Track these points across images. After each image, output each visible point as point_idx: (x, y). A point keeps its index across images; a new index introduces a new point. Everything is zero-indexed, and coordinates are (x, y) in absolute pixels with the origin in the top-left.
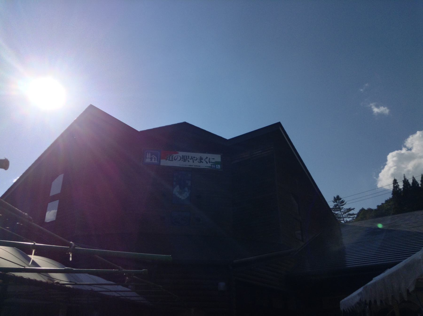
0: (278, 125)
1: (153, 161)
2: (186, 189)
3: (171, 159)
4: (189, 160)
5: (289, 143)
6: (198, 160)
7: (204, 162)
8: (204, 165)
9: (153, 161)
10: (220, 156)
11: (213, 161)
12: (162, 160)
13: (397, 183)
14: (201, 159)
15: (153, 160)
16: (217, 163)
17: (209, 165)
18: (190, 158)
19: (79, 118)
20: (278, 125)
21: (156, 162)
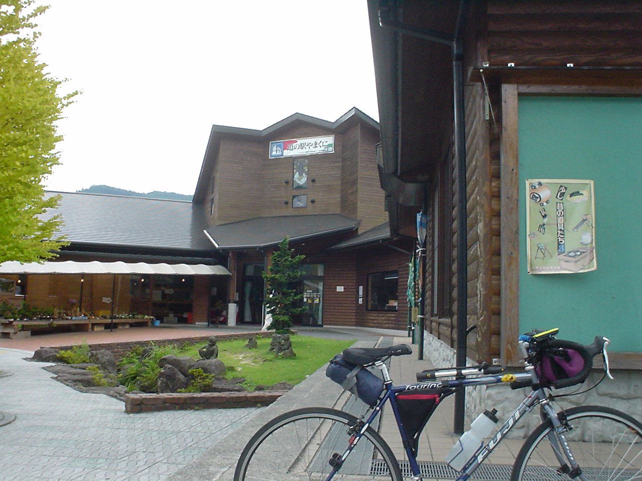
0: (213, 125)
1: (278, 153)
2: (304, 175)
3: (291, 149)
4: (306, 146)
5: (120, 268)
6: (313, 145)
7: (319, 147)
8: (318, 150)
9: (278, 153)
10: (502, 85)
11: (326, 144)
12: (284, 151)
13: (360, 225)
14: (316, 143)
15: (278, 151)
16: (330, 145)
17: (323, 148)
18: (307, 144)
19: (374, 63)
20: (213, 125)
21: (280, 153)
